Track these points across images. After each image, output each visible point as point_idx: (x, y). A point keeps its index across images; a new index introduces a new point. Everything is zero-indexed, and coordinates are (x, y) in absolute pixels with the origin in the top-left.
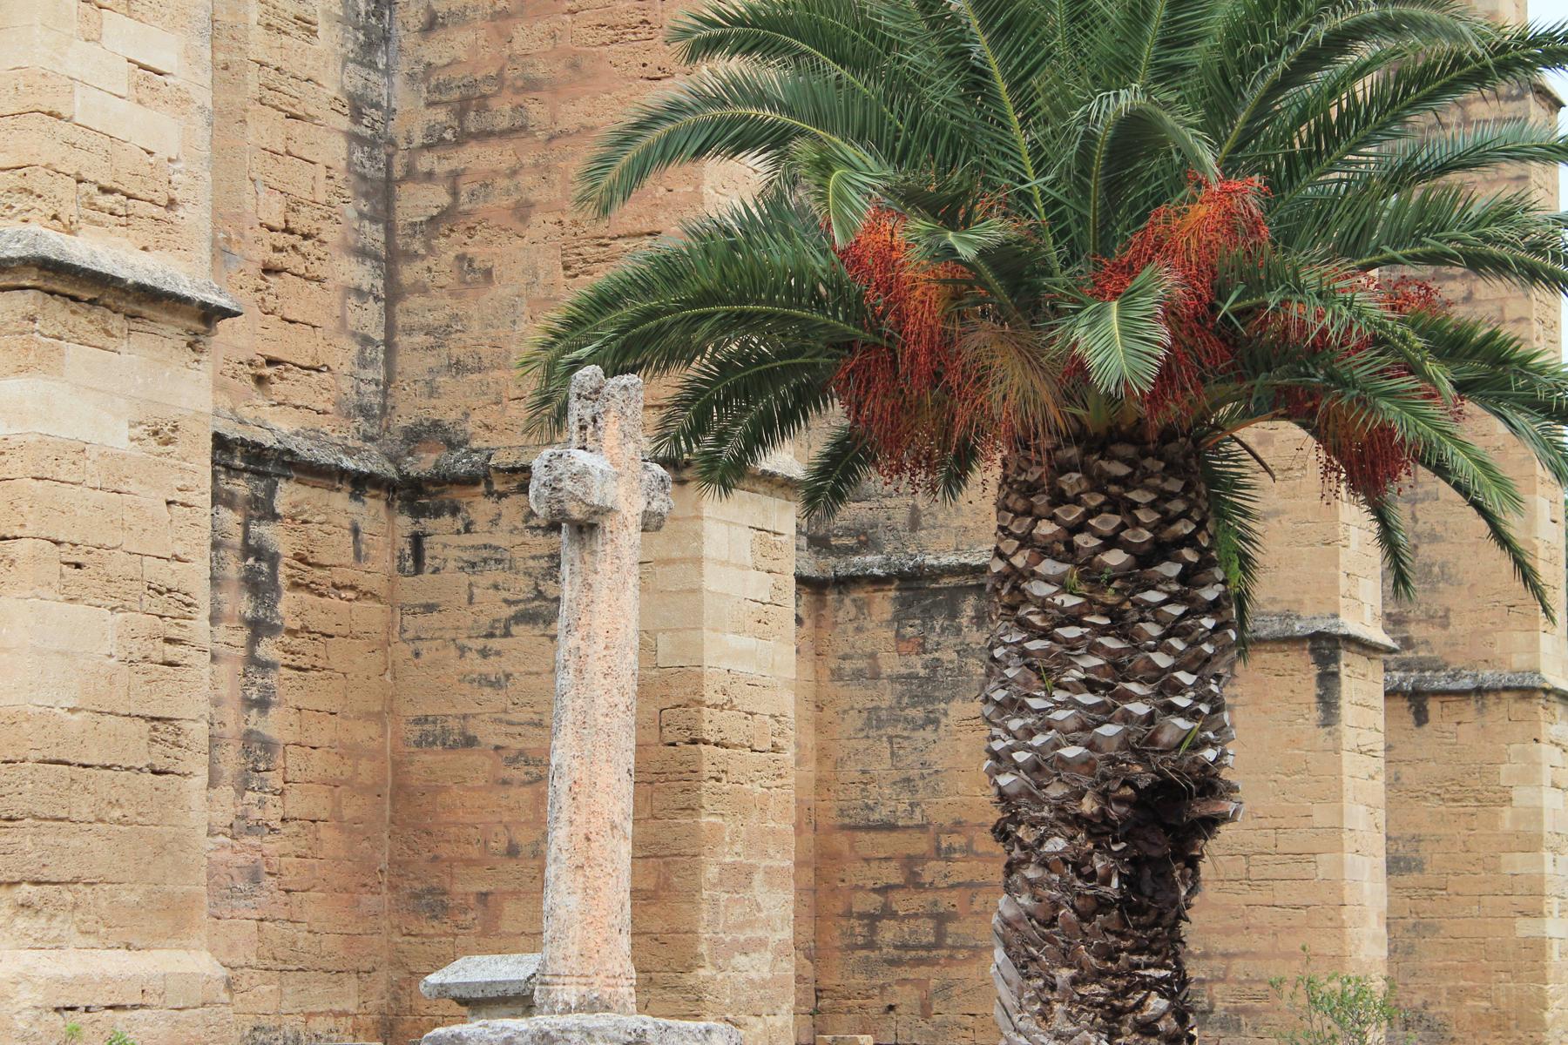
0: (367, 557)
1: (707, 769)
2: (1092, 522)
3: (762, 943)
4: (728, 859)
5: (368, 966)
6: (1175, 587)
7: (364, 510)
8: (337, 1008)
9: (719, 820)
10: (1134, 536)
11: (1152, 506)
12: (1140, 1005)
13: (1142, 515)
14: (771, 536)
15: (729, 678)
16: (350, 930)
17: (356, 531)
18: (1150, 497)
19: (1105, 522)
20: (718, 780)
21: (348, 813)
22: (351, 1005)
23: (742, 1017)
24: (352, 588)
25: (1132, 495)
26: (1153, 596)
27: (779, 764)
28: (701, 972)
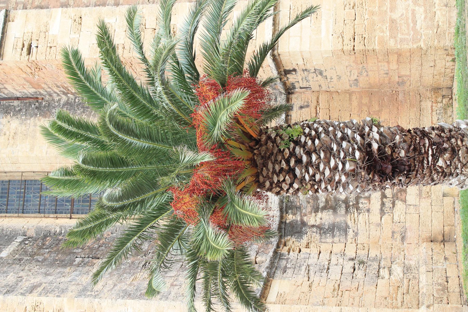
0: (308, 102)
1: (362, 47)
2: (286, 157)
3: (413, 11)
4: (388, 34)
5: (418, 97)
6: (303, 171)
7: (295, 104)
8: (430, 111)
9: (377, 38)
10: (288, 181)
11: (278, 176)
12: (441, 167)
13: (281, 179)
14: (291, 11)
15: (334, 35)
16: (409, 106)
17: (301, 107)
18: (275, 176)
19: (285, 187)
20: (365, 38)
21: (377, 108)
22: (429, 104)
23: (436, 23)
24: (316, 108)
25: (276, 182)
26: (307, 177)
27: (359, 5)
28: (422, 46)
